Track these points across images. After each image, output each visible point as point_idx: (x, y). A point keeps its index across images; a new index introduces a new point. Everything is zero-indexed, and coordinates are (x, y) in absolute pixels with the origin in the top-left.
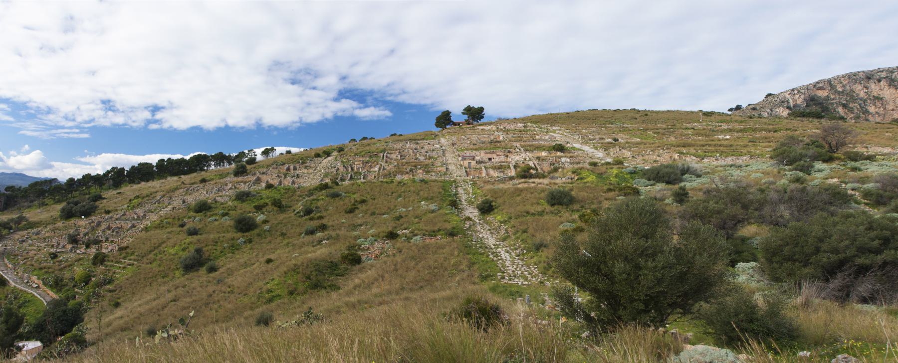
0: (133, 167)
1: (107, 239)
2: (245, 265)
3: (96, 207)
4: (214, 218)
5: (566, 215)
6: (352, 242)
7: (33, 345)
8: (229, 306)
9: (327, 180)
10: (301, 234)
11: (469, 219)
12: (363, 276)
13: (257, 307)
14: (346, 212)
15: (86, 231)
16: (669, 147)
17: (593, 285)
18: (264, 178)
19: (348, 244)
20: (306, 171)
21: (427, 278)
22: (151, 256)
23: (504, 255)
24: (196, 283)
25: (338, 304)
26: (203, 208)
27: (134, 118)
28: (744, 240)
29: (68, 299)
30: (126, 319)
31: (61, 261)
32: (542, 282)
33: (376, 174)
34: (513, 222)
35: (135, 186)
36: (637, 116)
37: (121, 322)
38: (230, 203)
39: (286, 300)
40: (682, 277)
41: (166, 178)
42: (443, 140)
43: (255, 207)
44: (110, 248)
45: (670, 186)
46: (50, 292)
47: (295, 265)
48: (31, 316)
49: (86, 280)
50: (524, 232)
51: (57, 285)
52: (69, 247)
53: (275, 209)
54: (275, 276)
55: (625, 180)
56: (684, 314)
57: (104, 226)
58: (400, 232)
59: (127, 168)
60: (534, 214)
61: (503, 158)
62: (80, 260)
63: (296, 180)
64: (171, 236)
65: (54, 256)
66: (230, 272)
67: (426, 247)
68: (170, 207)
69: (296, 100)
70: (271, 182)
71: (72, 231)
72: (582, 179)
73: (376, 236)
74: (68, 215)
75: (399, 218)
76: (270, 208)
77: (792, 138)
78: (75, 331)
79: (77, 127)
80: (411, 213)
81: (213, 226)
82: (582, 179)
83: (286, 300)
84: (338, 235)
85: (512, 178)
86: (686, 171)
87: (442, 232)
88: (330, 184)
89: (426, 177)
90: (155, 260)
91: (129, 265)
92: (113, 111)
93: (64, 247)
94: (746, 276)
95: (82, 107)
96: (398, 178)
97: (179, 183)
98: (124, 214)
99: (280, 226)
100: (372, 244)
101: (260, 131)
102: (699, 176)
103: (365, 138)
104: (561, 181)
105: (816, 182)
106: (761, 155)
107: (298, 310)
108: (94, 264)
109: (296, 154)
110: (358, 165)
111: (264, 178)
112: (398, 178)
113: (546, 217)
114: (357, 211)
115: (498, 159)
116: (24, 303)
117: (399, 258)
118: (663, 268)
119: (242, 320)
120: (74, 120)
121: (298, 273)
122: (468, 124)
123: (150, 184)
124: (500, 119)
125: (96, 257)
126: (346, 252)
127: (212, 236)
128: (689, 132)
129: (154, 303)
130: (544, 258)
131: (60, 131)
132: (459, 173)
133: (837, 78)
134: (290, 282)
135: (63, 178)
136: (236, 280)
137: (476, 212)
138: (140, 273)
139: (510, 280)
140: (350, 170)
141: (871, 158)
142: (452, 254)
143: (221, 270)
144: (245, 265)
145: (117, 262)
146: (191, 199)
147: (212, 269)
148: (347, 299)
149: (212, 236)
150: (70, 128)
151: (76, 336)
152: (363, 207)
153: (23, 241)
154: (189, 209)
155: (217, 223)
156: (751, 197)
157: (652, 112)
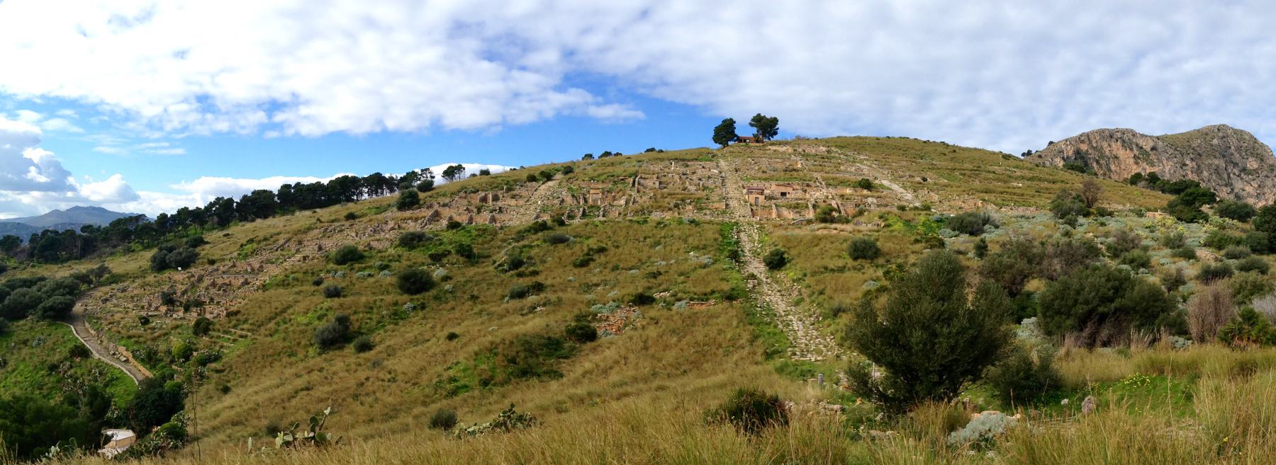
0: (245, 197)
1: (212, 300)
2: (415, 342)
3: (197, 255)
4: (366, 273)
5: (870, 271)
6: (584, 309)
7: (123, 436)
8: (390, 399)
9: (546, 218)
10: (503, 297)
11: (753, 276)
12: (596, 358)
13: (433, 402)
14: (576, 266)
15: (184, 288)
16: (971, 192)
17: (889, 359)
18: (446, 212)
19: (576, 312)
20: (513, 202)
21: (692, 359)
22: (272, 325)
23: (796, 325)
24: (339, 365)
25: (560, 398)
26: (350, 257)
27: (243, 122)
28: (1029, 295)
29: (164, 378)
30: (238, 409)
31: (154, 328)
32: (838, 356)
33: (621, 209)
34: (808, 280)
35: (249, 225)
36: (946, 151)
37: (232, 413)
38: (391, 251)
39: (476, 393)
40: (973, 342)
41: (293, 213)
42: (722, 163)
43: (431, 256)
44: (216, 312)
45: (973, 238)
46: (141, 368)
47: (492, 343)
48: (121, 398)
49: (186, 354)
50: (821, 293)
51: (150, 359)
52: (163, 309)
53: (462, 259)
54: (461, 359)
55: (931, 229)
56: (974, 381)
57: (207, 282)
58: (657, 296)
59: (237, 199)
60: (832, 270)
61: (800, 194)
62: (177, 327)
63: (497, 216)
64: (299, 298)
65: (145, 321)
66: (391, 352)
67: (693, 318)
68: (299, 256)
69: (498, 86)
70: (457, 219)
71: (166, 288)
72: (888, 226)
73: (619, 302)
74: (161, 265)
75: (655, 275)
76: (453, 257)
77: (1064, 190)
78: (173, 421)
79: (166, 139)
80: (674, 268)
81: (365, 284)
82: (888, 226)
83: (476, 393)
84: (560, 300)
85: (809, 222)
86: (986, 221)
87: (716, 295)
88: (549, 223)
89: (698, 217)
90: (277, 331)
91: (241, 336)
92: (213, 112)
93: (157, 309)
94: (1027, 334)
95: (172, 109)
96: (656, 216)
97: (314, 220)
98: (234, 266)
99: (470, 285)
100: (612, 311)
101: (437, 133)
102: (997, 227)
103: (607, 154)
104: (865, 228)
105: (1079, 236)
106: (1043, 207)
107: (494, 407)
108: (196, 333)
109: (496, 177)
110: (594, 196)
111: (446, 212)
112: (656, 216)
113: (847, 274)
114: (592, 265)
115: (794, 194)
116: (112, 380)
117: (652, 332)
118: (958, 333)
119: (410, 420)
120: (161, 129)
121: (496, 354)
122: (757, 141)
123: (270, 221)
124: (799, 138)
125: (198, 324)
126: (573, 324)
127: (363, 299)
128: (991, 176)
129: (277, 392)
130: (841, 325)
131: (145, 145)
132: (742, 212)
133: (1092, 132)
134: (483, 367)
135: (152, 214)
136: (402, 363)
137: (762, 267)
138: (256, 349)
139: (802, 356)
140: (582, 202)
141: (1111, 214)
142: (729, 325)
143: (378, 348)
144: (415, 342)
145: (226, 332)
146: (333, 244)
147: (365, 347)
148: (572, 391)
149: (363, 299)
150: (157, 140)
151: (175, 427)
152: (601, 259)
153: (107, 300)
154: (328, 259)
155: (371, 280)
156: (1035, 250)
157: (960, 148)
